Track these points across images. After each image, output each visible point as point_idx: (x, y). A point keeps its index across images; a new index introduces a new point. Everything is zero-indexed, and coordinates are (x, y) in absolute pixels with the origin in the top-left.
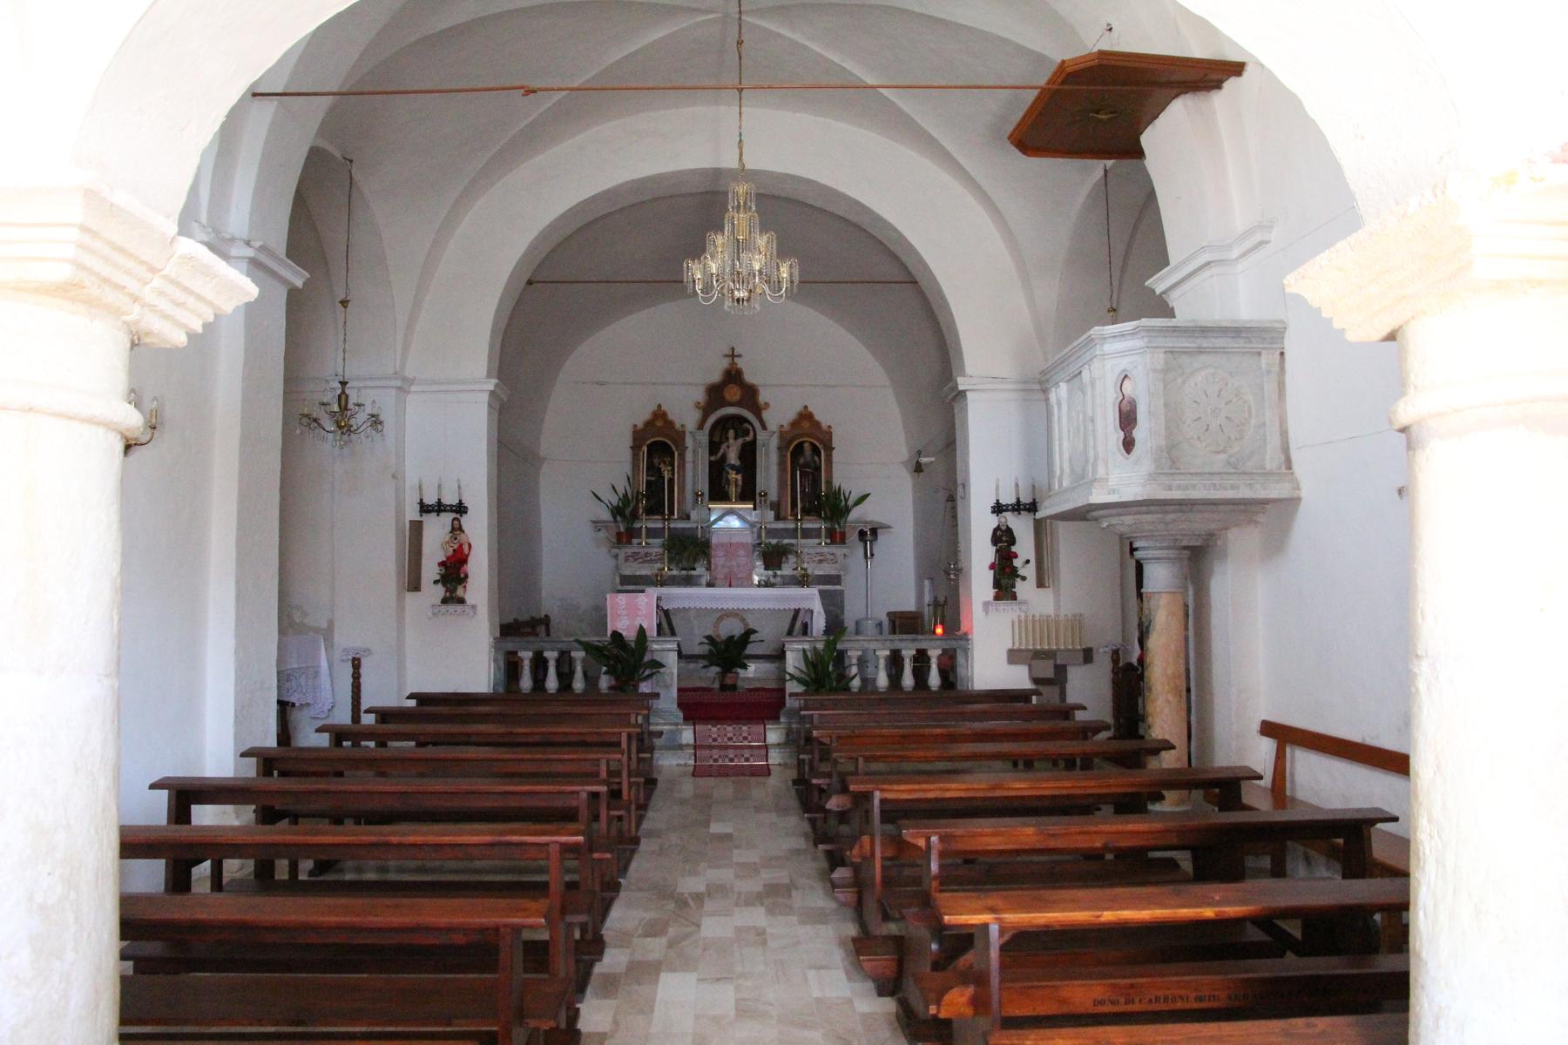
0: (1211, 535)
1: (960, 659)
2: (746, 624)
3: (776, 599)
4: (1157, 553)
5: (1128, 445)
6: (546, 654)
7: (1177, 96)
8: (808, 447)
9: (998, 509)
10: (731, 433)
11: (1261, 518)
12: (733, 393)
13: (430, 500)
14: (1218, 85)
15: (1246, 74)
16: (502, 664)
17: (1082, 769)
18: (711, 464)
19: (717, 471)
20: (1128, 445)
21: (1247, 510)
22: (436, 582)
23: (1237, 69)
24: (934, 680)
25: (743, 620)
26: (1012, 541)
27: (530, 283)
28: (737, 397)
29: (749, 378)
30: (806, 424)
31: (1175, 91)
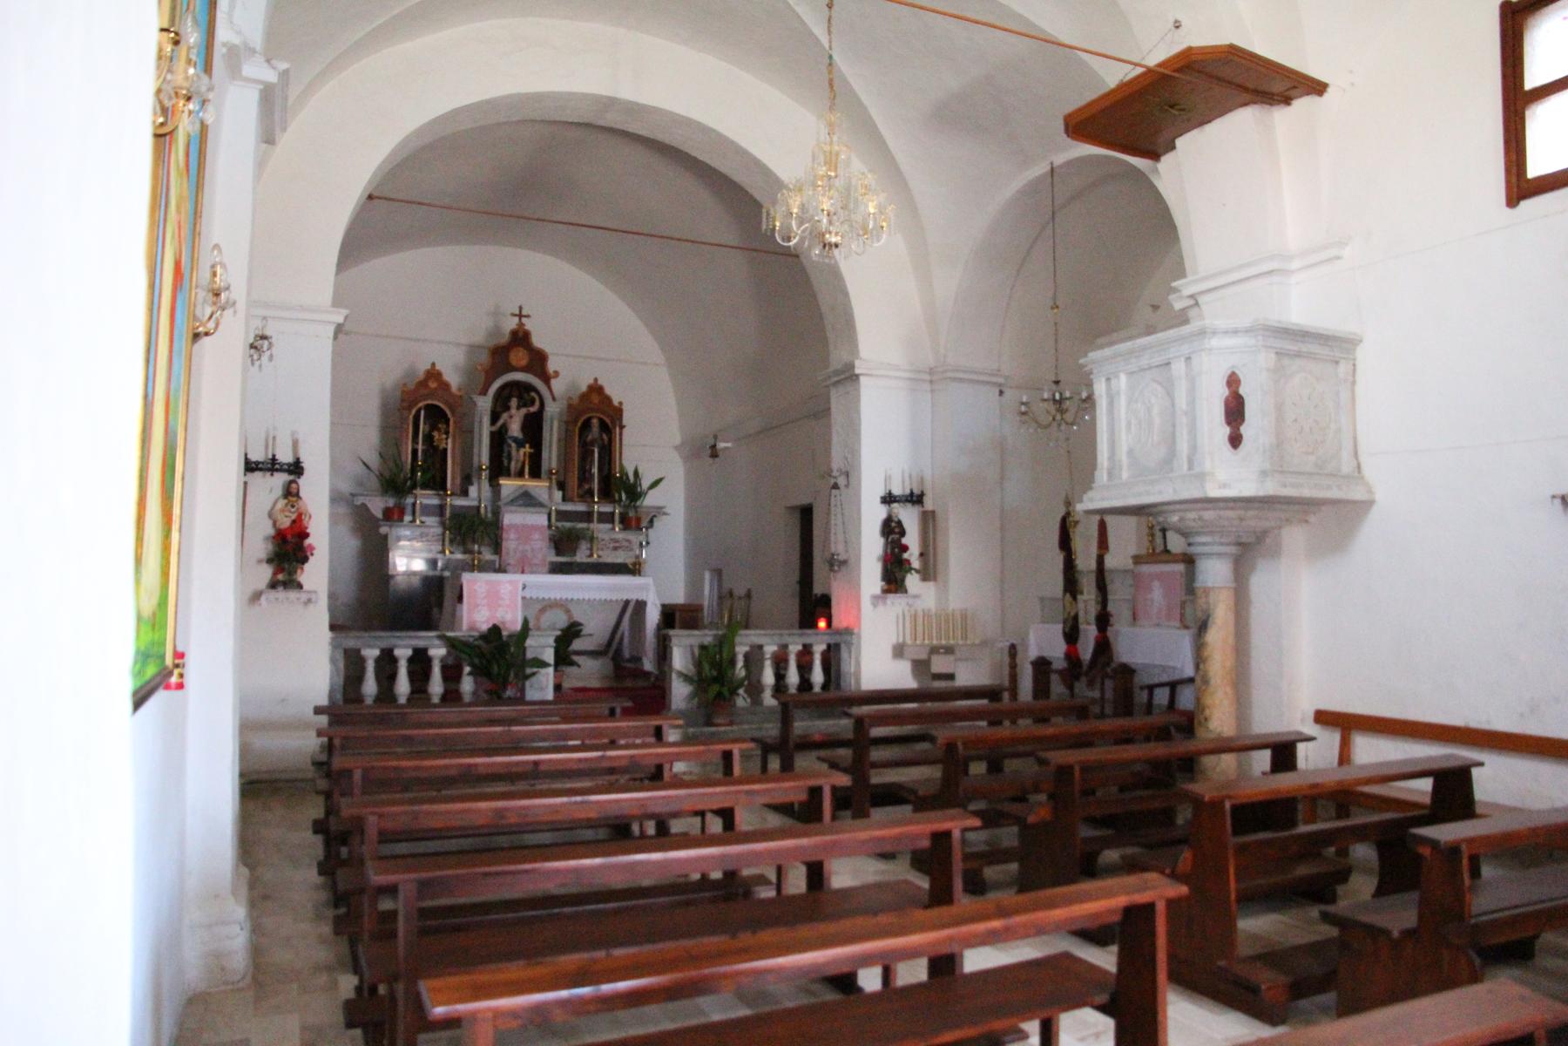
0: (1265, 533)
1: (844, 654)
2: (570, 616)
3: (612, 588)
4: (1217, 549)
5: (1235, 441)
6: (397, 652)
7: (1245, 104)
8: (597, 420)
9: (888, 499)
10: (514, 402)
11: (1312, 519)
12: (519, 357)
13: (257, 455)
14: (1287, 100)
15: (1326, 95)
16: (341, 665)
17: (1071, 767)
18: (492, 434)
19: (499, 439)
20: (1235, 441)
21: (1302, 507)
22: (260, 561)
23: (1317, 88)
24: (818, 676)
25: (568, 611)
26: (903, 533)
27: (370, 197)
28: (524, 362)
29: (537, 341)
30: (595, 399)
31: (1247, 97)
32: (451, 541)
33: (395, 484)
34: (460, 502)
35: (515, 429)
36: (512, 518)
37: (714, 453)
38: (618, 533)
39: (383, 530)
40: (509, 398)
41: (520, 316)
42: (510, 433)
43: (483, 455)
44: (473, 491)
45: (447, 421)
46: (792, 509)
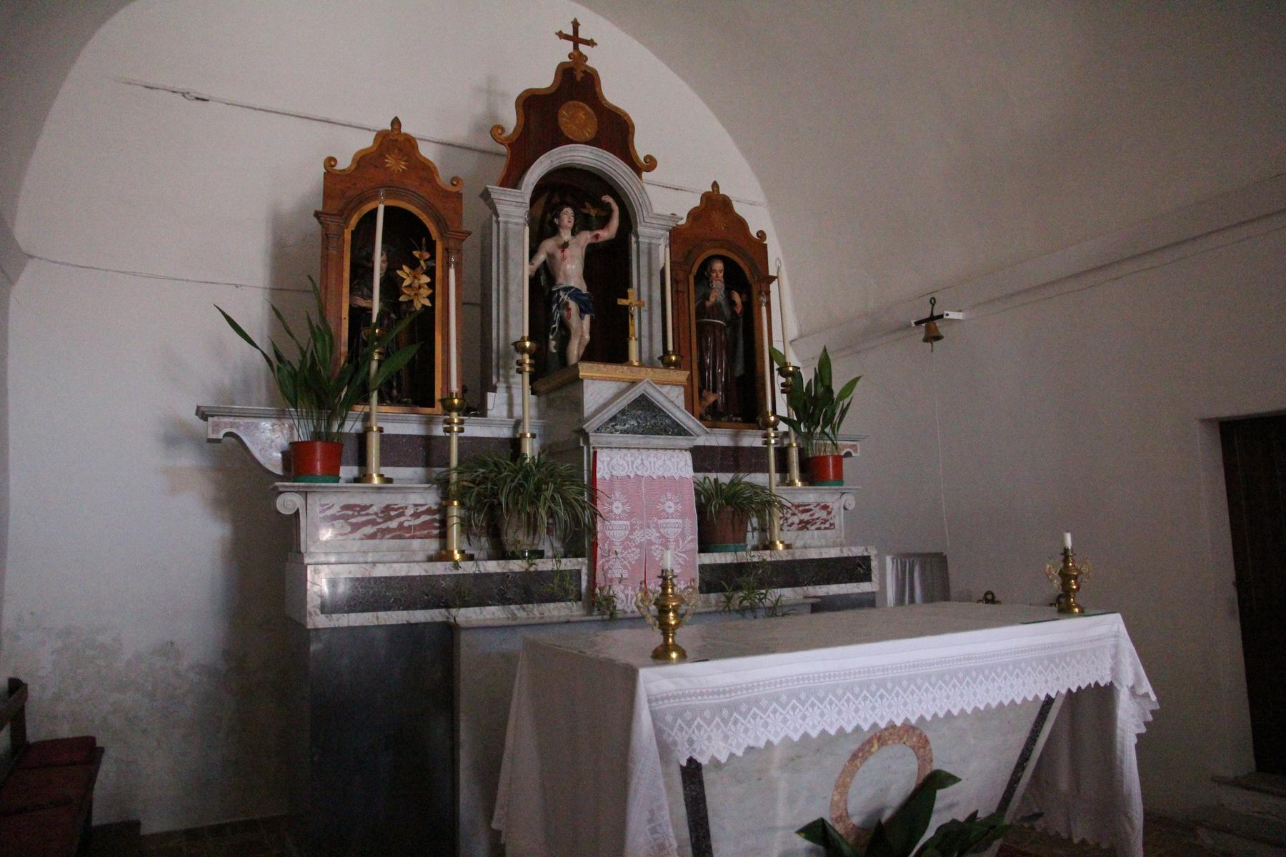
3: (1053, 658)
12: (574, 116)
29: (612, 93)
32: (466, 527)
33: (312, 379)
34: (475, 429)
35: (572, 272)
36: (619, 463)
37: (931, 327)
38: (800, 493)
39: (287, 503)
40: (555, 210)
41: (575, 39)
42: (562, 282)
43: (514, 319)
44: (496, 402)
45: (431, 247)
46: (1207, 421)
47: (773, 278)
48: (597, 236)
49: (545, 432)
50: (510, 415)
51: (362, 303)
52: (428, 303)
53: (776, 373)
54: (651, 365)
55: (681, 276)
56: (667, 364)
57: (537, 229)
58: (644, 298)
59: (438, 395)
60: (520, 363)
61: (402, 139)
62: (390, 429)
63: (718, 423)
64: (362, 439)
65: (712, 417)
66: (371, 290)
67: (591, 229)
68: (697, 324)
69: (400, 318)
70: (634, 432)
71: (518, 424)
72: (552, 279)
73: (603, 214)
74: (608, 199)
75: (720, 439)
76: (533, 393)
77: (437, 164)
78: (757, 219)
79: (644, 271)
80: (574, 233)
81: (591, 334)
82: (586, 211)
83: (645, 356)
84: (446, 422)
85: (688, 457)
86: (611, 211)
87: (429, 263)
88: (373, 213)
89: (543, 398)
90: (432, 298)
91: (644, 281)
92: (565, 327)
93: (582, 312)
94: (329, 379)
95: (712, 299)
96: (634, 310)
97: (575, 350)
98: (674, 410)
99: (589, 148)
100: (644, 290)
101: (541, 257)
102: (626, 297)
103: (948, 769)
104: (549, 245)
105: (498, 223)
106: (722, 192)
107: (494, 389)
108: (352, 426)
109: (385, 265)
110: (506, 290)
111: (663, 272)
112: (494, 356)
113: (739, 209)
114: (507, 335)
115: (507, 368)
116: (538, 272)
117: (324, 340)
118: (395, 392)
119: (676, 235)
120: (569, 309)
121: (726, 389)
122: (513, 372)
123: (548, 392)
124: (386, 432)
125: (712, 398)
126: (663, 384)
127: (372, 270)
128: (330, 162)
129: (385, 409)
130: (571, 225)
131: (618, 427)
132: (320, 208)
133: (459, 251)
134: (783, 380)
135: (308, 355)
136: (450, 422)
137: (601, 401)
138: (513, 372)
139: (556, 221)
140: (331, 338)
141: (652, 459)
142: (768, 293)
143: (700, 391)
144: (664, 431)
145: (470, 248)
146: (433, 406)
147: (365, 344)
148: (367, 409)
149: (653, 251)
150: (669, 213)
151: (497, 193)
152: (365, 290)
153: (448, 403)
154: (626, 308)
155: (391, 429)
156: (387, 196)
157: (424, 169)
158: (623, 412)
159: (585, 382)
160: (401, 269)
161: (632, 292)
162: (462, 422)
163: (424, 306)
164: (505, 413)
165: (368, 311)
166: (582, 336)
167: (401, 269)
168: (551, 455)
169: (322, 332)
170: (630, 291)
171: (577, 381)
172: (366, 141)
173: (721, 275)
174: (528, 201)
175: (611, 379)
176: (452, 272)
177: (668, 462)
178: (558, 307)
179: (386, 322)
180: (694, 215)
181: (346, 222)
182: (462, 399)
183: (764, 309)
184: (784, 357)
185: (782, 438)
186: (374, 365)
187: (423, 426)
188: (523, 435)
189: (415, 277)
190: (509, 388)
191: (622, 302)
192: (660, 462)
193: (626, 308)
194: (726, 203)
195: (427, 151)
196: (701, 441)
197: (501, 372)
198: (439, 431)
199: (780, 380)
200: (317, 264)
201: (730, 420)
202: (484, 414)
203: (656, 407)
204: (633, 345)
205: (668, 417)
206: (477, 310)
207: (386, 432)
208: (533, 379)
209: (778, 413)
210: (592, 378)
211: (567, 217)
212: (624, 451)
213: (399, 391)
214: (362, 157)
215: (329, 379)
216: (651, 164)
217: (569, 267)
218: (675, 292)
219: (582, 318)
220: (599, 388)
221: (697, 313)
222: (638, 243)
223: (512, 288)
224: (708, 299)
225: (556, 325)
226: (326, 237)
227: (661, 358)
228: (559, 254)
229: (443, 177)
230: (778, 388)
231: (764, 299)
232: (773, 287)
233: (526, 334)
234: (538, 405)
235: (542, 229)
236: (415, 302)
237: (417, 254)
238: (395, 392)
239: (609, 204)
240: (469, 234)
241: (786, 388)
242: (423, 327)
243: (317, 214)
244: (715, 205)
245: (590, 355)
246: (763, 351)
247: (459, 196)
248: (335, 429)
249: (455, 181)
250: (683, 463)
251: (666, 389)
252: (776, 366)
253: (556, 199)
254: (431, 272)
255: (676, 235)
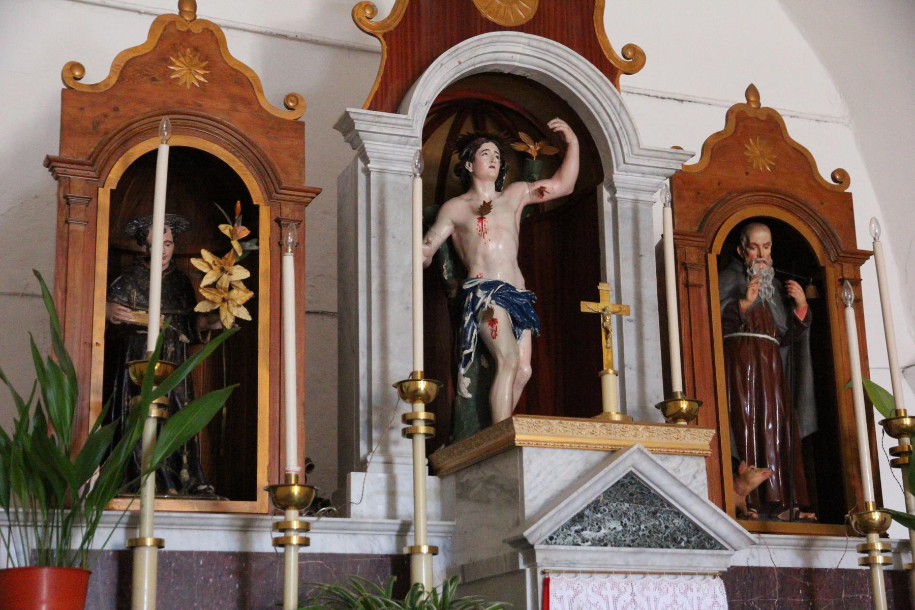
34: (329, 539)
35: (497, 256)
40: (466, 147)
42: (480, 272)
43: (397, 342)
44: (366, 489)
45: (251, 218)
47: (866, 255)
48: (541, 191)
49: (457, 539)
50: (392, 512)
51: (129, 316)
52: (245, 315)
53: (879, 429)
54: (645, 419)
55: (693, 257)
56: (673, 418)
57: (434, 180)
58: (628, 299)
59: (262, 479)
60: (409, 420)
61: (197, 29)
62: (176, 541)
63: (772, 524)
64: (125, 561)
65: (760, 511)
66: (145, 293)
67: (532, 180)
68: (726, 343)
69: (195, 342)
70: (617, 543)
71: (405, 529)
72: (462, 270)
73: (552, 151)
74: (558, 125)
75: (778, 552)
76: (432, 472)
77: (258, 71)
78: (829, 144)
79: (626, 251)
80: (500, 186)
81: (534, 363)
82: (520, 147)
83: (632, 402)
84: (278, 527)
85: (718, 588)
86: (564, 146)
87: (248, 245)
88: (151, 158)
89: (451, 482)
90: (252, 306)
91: (627, 268)
92: (486, 351)
93: (517, 325)
94: (68, 454)
95: (752, 296)
96: (611, 322)
97: (505, 393)
98: (689, 501)
99: (524, 37)
100: (628, 284)
101: (443, 230)
102: (597, 299)
103: (176, 415)
104: (456, 209)
105: (367, 172)
106: (764, 103)
107: (362, 467)
108: (108, 537)
109: (170, 250)
110: (383, 292)
111: (660, 251)
112: (362, 407)
113: (796, 132)
114: (385, 372)
115: (386, 427)
116: (437, 258)
117: (60, 386)
118: (185, 474)
119: (682, 185)
120: (493, 322)
121: (783, 458)
122: (396, 434)
123: (457, 471)
124: (168, 547)
125: (757, 478)
126: (669, 453)
127: (148, 258)
128: (73, 71)
129: (167, 504)
130: (495, 173)
131: (587, 534)
132: (55, 152)
133: (300, 222)
134: (894, 443)
135: (32, 411)
136: (283, 527)
137: (556, 486)
138: (396, 434)
139: (469, 167)
140: (74, 380)
141: (652, 593)
142: (856, 282)
143: (736, 464)
144: (672, 541)
145: (320, 218)
146: (252, 497)
147: (135, 390)
148: (135, 505)
149: (641, 216)
150: (668, 147)
151: (368, 122)
152: (135, 294)
153: (280, 492)
154: (596, 318)
155: (179, 541)
156: (176, 129)
157: (238, 83)
158: (595, 506)
159: (526, 452)
160: (199, 256)
161: (606, 289)
162: (306, 528)
163: (238, 320)
164: (381, 508)
165: (139, 332)
166: (517, 369)
167: (199, 256)
168: (464, 586)
169: (57, 371)
170: (601, 287)
171: (510, 449)
172: (135, 34)
173: (767, 252)
174: (419, 133)
175: (572, 447)
176: (289, 261)
177: (681, 599)
178: (474, 318)
179: (171, 348)
180: (716, 148)
181: (102, 174)
182: (307, 486)
183: (850, 313)
184: (893, 399)
185: (897, 553)
186: (150, 427)
187: (236, 536)
188: (415, 550)
189: (223, 270)
190: (389, 464)
191: (587, 307)
192: (667, 599)
193: (596, 318)
194: (772, 124)
195: (241, 50)
196: (743, 557)
197: (375, 435)
198: (263, 543)
199: (886, 442)
200: (49, 246)
201: (794, 518)
202: (344, 512)
203: (657, 496)
204: (610, 384)
205: (678, 514)
206: (331, 324)
207: (168, 547)
208: (431, 447)
209: (886, 505)
210: (538, 445)
211: (488, 159)
212: (599, 578)
213: (193, 470)
214: (128, 64)
215: (68, 454)
216: (635, 59)
217: (492, 246)
218: (684, 286)
219: (516, 336)
220: (553, 461)
221: (724, 320)
222: (614, 201)
223: (394, 286)
224: (744, 297)
225: (472, 349)
226: (66, 203)
227: (662, 407)
228: (474, 224)
229: (271, 96)
230: (884, 460)
231: (849, 295)
232: (867, 270)
233: (420, 367)
234: (441, 494)
235: (445, 181)
236: (224, 314)
237: (225, 229)
238: (185, 474)
239: (561, 134)
240: (317, 192)
241: (899, 458)
242: (237, 357)
243: (50, 163)
244: (752, 125)
245: (532, 402)
246: (851, 391)
247: (298, 127)
248: (76, 543)
249: (292, 101)
250: (709, 601)
251: (672, 463)
252: (878, 417)
253: (467, 128)
254: (250, 261)
255: (682, 185)
